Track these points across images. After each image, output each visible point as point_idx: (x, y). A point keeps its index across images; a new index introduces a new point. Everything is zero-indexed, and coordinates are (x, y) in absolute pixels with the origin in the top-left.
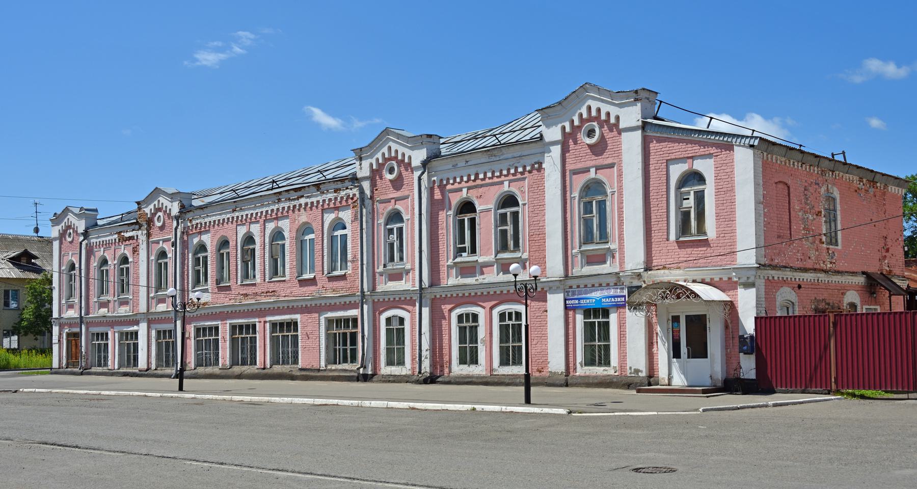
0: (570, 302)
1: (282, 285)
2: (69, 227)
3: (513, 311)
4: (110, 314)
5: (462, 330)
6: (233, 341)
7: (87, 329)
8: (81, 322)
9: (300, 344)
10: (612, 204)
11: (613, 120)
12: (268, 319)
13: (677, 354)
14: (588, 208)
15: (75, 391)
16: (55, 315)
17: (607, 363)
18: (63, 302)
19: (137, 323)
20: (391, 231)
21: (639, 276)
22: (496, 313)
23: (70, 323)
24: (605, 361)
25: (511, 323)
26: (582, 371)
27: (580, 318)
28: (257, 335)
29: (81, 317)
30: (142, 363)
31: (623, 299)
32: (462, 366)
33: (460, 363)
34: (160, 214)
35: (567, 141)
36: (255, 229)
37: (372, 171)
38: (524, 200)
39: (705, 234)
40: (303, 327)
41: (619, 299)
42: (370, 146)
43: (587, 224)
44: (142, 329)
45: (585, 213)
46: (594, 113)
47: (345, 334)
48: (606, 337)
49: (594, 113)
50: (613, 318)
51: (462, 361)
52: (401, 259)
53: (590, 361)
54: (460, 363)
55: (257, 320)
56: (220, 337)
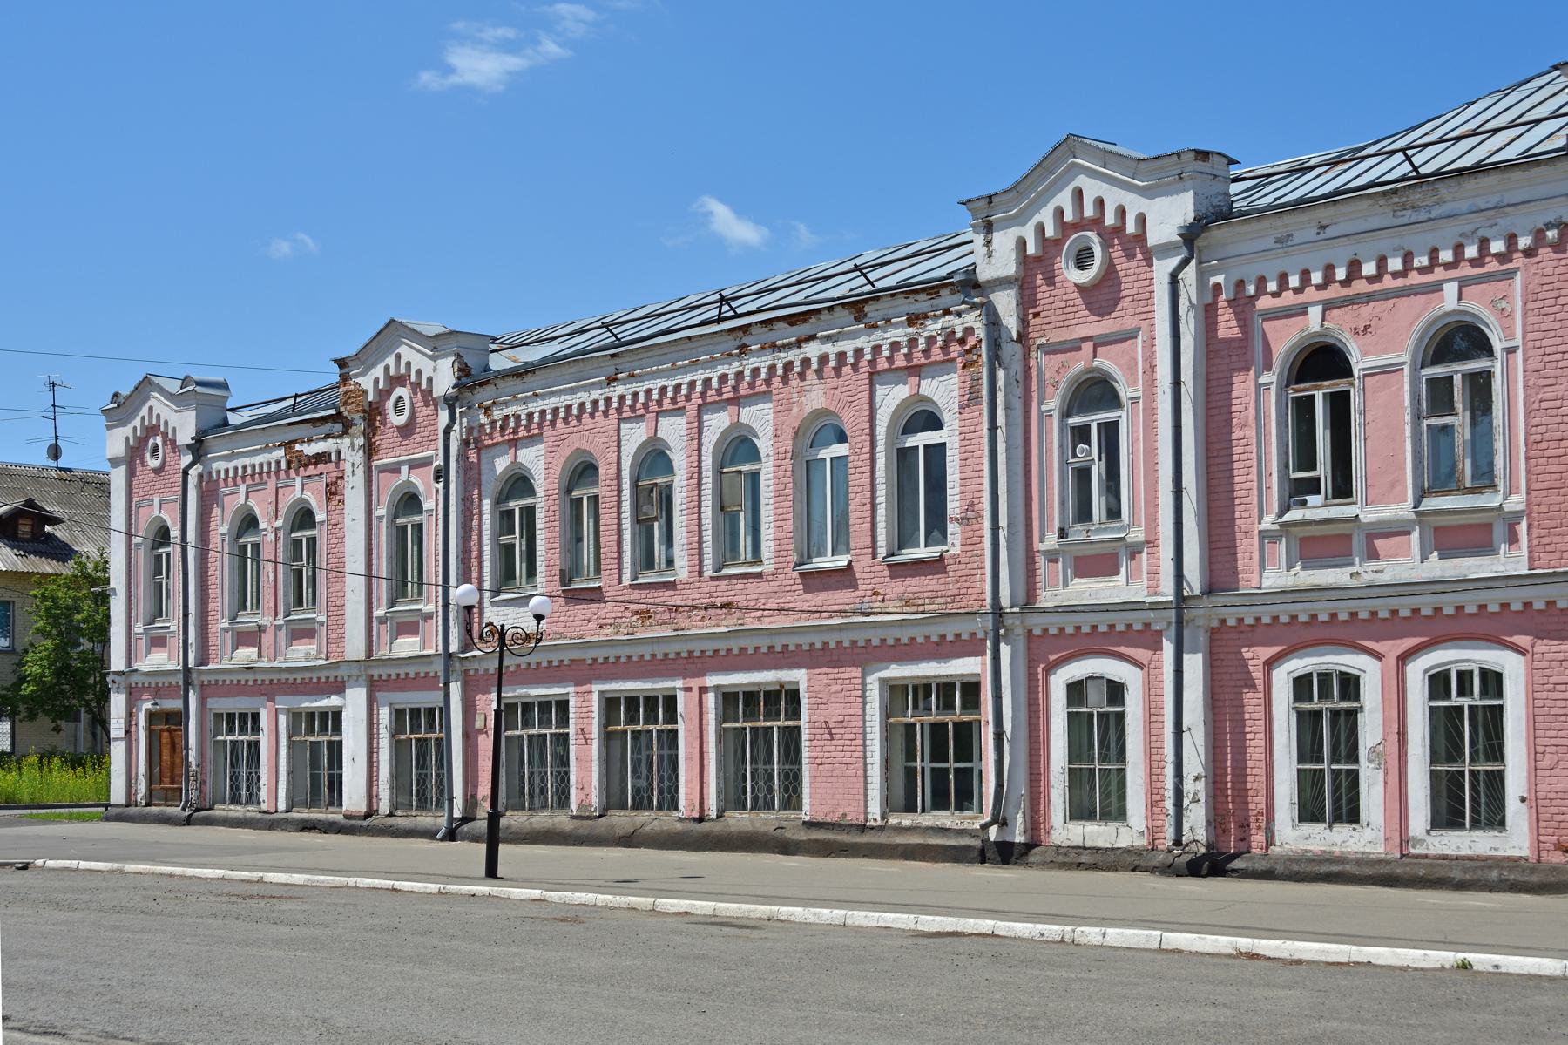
1: (752, 586)
2: (152, 430)
4: (264, 664)
6: (731, 743)
8: (187, 683)
9: (805, 753)
11: (1131, 228)
12: (712, 680)
16: (117, 662)
18: (138, 628)
19: (339, 688)
22: (1416, 672)
23: (157, 685)
28: (680, 727)
29: (187, 670)
30: (353, 797)
36: (674, 431)
44: (353, 703)
46: (1089, 211)
47: (938, 730)
49: (1089, 211)
51: (1309, 812)
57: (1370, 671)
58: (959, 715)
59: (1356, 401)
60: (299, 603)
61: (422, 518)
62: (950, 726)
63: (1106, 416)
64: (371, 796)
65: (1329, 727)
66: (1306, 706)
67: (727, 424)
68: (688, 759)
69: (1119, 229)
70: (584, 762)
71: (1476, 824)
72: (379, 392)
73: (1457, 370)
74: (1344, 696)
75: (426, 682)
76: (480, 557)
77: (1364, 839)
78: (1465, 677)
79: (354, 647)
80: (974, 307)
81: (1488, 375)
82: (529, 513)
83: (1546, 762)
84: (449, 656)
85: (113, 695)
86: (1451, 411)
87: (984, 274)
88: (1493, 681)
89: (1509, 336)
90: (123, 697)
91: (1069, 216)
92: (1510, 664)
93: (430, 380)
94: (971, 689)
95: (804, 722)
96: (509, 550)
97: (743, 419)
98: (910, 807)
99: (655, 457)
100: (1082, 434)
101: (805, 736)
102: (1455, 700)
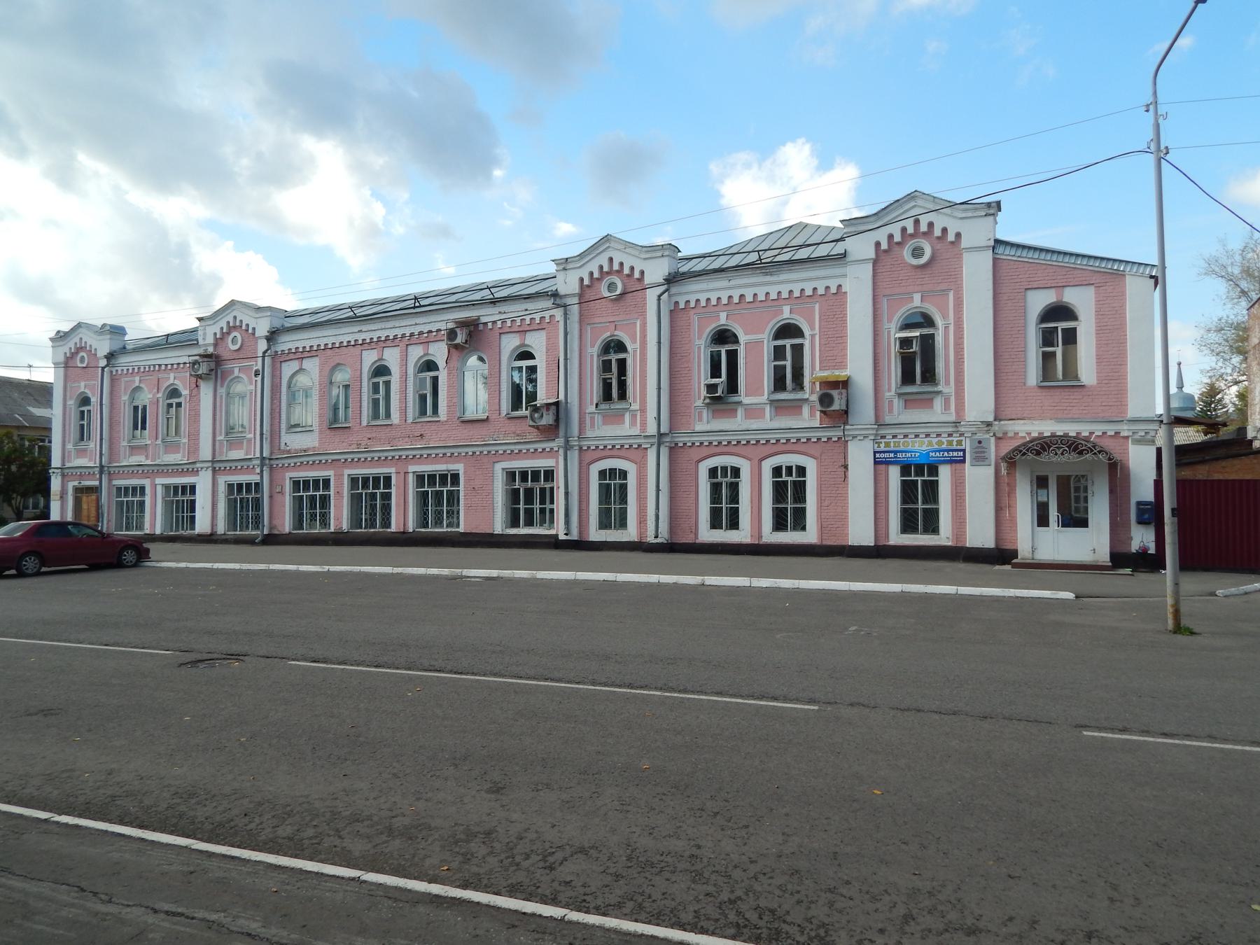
0: (882, 455)
1: (434, 427)
2: (80, 349)
3: (729, 465)
4: (149, 462)
5: (716, 488)
6: (356, 500)
7: (110, 480)
8: (101, 473)
9: (462, 502)
10: (634, 360)
11: (637, 275)
12: (412, 468)
13: (1043, 521)
14: (376, 388)
15: (506, 573)
16: (56, 461)
17: (935, 531)
18: (70, 446)
19: (195, 472)
20: (170, 405)
21: (989, 424)
22: (768, 466)
23: (83, 472)
24: (932, 526)
25: (789, 479)
26: (896, 538)
27: (894, 473)
28: (393, 490)
29: (102, 467)
30: (202, 524)
31: (961, 454)
32: (603, 532)
33: (1086, 526)
34: (82, 354)
35: (881, 256)
36: (392, 357)
37: (216, 339)
38: (812, 328)
39: (1076, 378)
40: (467, 481)
41: (955, 454)
42: (582, 255)
43: (376, 403)
44: (203, 483)
45: (776, 359)
46: (616, 267)
47: (313, 498)
48: (623, 499)
49: (616, 267)
50: (945, 473)
51: (715, 524)
52: (177, 433)
53: (604, 524)
54: (600, 528)
55: (393, 470)
56: (332, 493)
57: (745, 467)
58: (187, 497)
59: (629, 363)
60: (82, 439)
61: (181, 400)
62: (1187, 473)
63: (177, 400)
64: (213, 524)
65: (725, 489)
66: (715, 480)
67: (518, 343)
68: (397, 505)
69: (630, 275)
70: (339, 508)
71: (794, 529)
72: (223, 334)
73: (787, 343)
74: (453, 484)
75: (250, 470)
76: (947, 356)
77: (742, 536)
78: (789, 469)
79: (205, 452)
80: (559, 306)
81: (802, 345)
82: (387, 384)
83: (826, 503)
84: (263, 459)
85: (53, 478)
86: (784, 359)
87: (562, 291)
88: (802, 471)
89: (812, 328)
90: (59, 478)
91: (606, 269)
92: (811, 466)
93: (642, 273)
94: (549, 475)
95: (461, 488)
96: (82, 426)
97: (527, 342)
98: (426, 526)
99: (381, 370)
100: (170, 405)
101: (462, 494)
102: (784, 478)
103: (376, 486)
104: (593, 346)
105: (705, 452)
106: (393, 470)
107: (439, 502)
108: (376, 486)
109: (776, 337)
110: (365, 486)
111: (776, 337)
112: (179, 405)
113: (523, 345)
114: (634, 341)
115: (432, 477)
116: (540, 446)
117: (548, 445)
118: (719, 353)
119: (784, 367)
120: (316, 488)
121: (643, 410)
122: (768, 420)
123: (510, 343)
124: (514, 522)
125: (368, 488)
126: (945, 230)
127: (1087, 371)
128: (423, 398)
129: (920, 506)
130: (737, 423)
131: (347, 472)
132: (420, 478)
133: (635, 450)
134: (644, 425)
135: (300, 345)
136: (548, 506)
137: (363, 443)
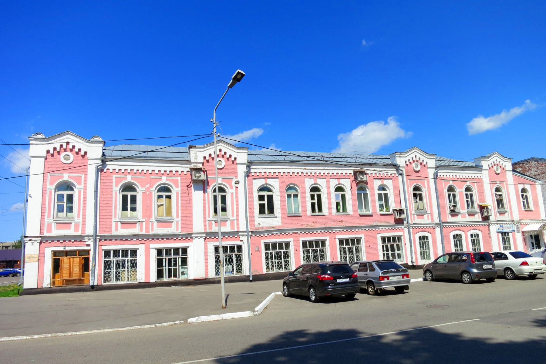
55: (328, 238)
86: (264, 200)
92: (480, 233)
103: (317, 245)
104: (116, 186)
105: (418, 230)
106: (328, 238)
107: (393, 249)
108: (317, 245)
109: (159, 191)
110: (347, 243)
111: (159, 191)
112: (296, 196)
113: (315, 184)
114: (80, 184)
115: (347, 241)
116: (397, 227)
117: (400, 227)
118: (127, 196)
119: (63, 205)
120: (353, 243)
121: (432, 214)
122: (468, 219)
123: (377, 183)
124: (105, 282)
125: (282, 248)
126: (230, 156)
127: (532, 207)
128: (338, 204)
129: (172, 268)
130: (459, 219)
131: (302, 239)
132: (341, 242)
133: (431, 227)
134: (432, 219)
135: (268, 171)
136: (385, 253)
137: (310, 224)
